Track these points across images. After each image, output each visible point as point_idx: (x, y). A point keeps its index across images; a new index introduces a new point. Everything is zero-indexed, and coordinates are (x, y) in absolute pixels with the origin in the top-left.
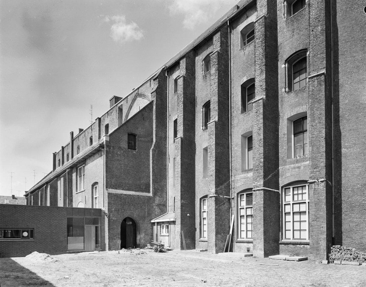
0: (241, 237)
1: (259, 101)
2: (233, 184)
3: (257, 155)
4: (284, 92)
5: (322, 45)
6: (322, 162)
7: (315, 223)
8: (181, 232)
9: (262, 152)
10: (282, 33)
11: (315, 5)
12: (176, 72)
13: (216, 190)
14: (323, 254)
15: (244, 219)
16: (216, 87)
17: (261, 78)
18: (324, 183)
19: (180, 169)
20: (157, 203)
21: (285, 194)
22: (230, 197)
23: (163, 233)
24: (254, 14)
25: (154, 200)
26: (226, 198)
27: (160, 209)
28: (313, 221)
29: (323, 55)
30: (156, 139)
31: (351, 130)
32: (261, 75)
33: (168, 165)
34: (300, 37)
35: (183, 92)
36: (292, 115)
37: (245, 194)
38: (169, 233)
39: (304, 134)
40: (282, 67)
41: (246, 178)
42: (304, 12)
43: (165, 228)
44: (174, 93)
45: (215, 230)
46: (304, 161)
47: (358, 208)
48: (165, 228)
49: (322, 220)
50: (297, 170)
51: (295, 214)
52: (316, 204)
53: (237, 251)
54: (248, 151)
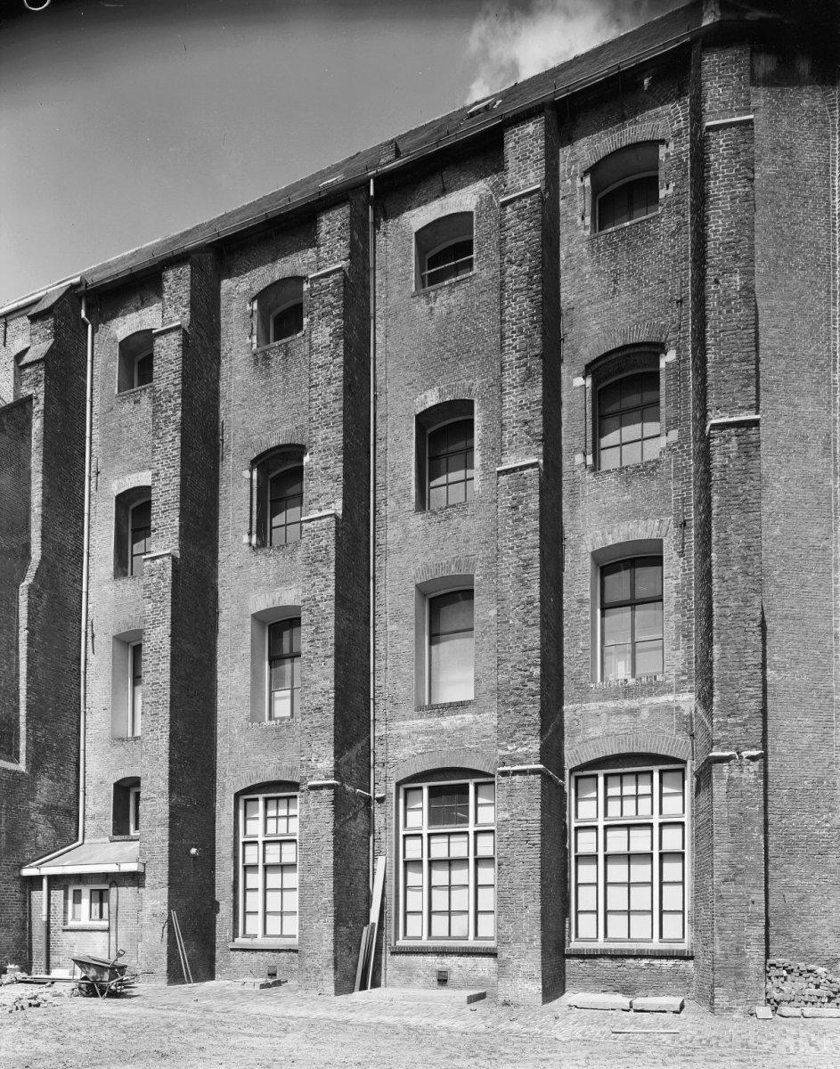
0: (661, 936)
1: (525, 472)
2: (379, 749)
3: (517, 655)
4: (579, 466)
5: (745, 336)
6: (751, 697)
7: (731, 887)
8: (170, 915)
9: (537, 644)
10: (576, 276)
11: (723, 203)
12: (128, 316)
13: (336, 765)
14: (755, 986)
15: (257, 872)
16: (336, 394)
17: (527, 395)
18: (758, 763)
19: (167, 677)
20: (43, 800)
21: (576, 795)
22: (371, 795)
23: (80, 920)
24: (471, 187)
25: (33, 790)
26: (361, 796)
27: (55, 826)
28: (726, 880)
29: (747, 367)
30: (43, 548)
31: (786, 617)
32: (526, 387)
33: (86, 660)
34: (640, 304)
35: (179, 387)
36: (610, 543)
37: (425, 786)
38: (112, 920)
39: (633, 610)
40: (576, 385)
41: (433, 733)
42: (656, 227)
43: (85, 901)
44: (119, 391)
45: (332, 909)
46: (650, 694)
47: (804, 847)
48: (85, 901)
49: (753, 881)
50: (626, 718)
51: (248, 869)
52: (733, 829)
53: (396, 981)
54: (431, 643)
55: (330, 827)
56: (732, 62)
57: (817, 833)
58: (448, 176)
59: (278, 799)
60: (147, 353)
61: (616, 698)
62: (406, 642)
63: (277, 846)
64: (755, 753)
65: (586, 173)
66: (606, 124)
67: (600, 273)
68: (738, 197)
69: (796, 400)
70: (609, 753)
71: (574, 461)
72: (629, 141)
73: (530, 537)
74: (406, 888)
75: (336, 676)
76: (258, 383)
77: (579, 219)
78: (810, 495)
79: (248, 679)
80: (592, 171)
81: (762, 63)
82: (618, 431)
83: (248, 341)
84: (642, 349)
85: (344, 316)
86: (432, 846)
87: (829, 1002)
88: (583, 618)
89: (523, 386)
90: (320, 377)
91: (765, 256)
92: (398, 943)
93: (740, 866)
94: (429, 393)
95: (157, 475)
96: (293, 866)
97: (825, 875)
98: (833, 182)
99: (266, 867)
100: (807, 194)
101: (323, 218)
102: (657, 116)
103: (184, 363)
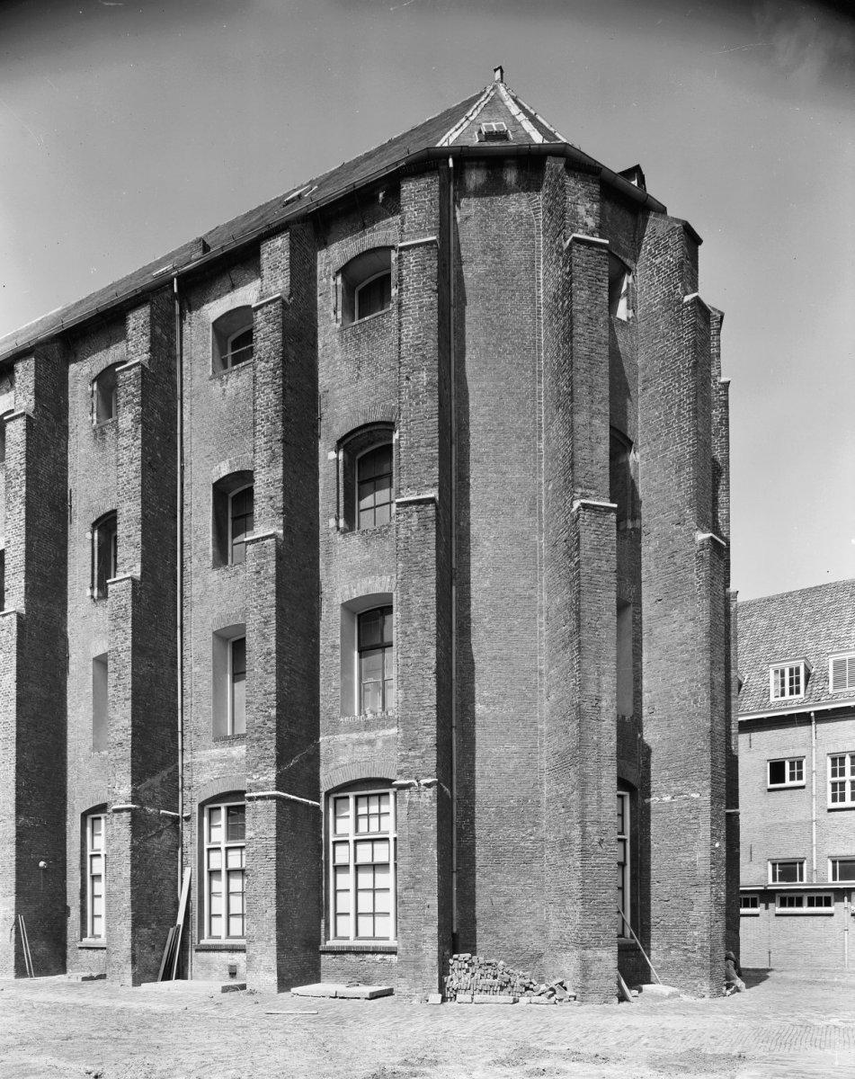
1: (265, 542)
2: (187, 774)
3: (260, 698)
4: (332, 529)
7: (411, 893)
8: (17, 920)
9: (274, 689)
10: (330, 363)
13: (134, 791)
15: (348, 872)
16: (136, 472)
18: (432, 789)
19: (13, 716)
22: (180, 814)
26: (166, 816)
28: (406, 889)
31: (495, 658)
34: (377, 388)
35: (24, 466)
36: (355, 596)
40: (329, 457)
46: (383, 726)
49: (428, 888)
50: (366, 748)
52: (412, 845)
53: (199, 974)
55: (128, 844)
56: (424, 189)
57: (522, 844)
58: (235, 274)
59: (368, 796)
60: (247, 329)
61: (358, 730)
62: (206, 682)
63: (369, 846)
64: (429, 781)
65: (337, 273)
66: (352, 231)
67: (348, 360)
68: (424, 306)
69: (504, 468)
70: (354, 778)
71: (329, 522)
72: (369, 247)
73: (269, 597)
74: (211, 894)
75: (133, 716)
76: (95, 455)
77: (333, 313)
78: (517, 550)
79: (91, 714)
80: (343, 271)
81: (474, 177)
82: (372, 496)
83: (90, 418)
84: (381, 427)
85: (142, 404)
86: (229, 858)
87: (501, 990)
88: (335, 661)
89: (269, 466)
90: (125, 456)
91: (477, 345)
92: (202, 942)
93: (418, 876)
94: (222, 464)
95: (8, 542)
96: (385, 866)
97: (530, 881)
98: (538, 276)
99: (357, 867)
100: (514, 288)
101: (130, 316)
102: (389, 226)
103: (28, 445)
